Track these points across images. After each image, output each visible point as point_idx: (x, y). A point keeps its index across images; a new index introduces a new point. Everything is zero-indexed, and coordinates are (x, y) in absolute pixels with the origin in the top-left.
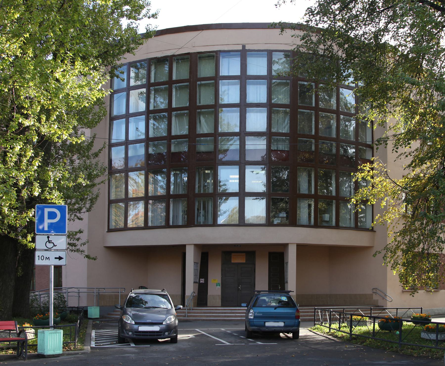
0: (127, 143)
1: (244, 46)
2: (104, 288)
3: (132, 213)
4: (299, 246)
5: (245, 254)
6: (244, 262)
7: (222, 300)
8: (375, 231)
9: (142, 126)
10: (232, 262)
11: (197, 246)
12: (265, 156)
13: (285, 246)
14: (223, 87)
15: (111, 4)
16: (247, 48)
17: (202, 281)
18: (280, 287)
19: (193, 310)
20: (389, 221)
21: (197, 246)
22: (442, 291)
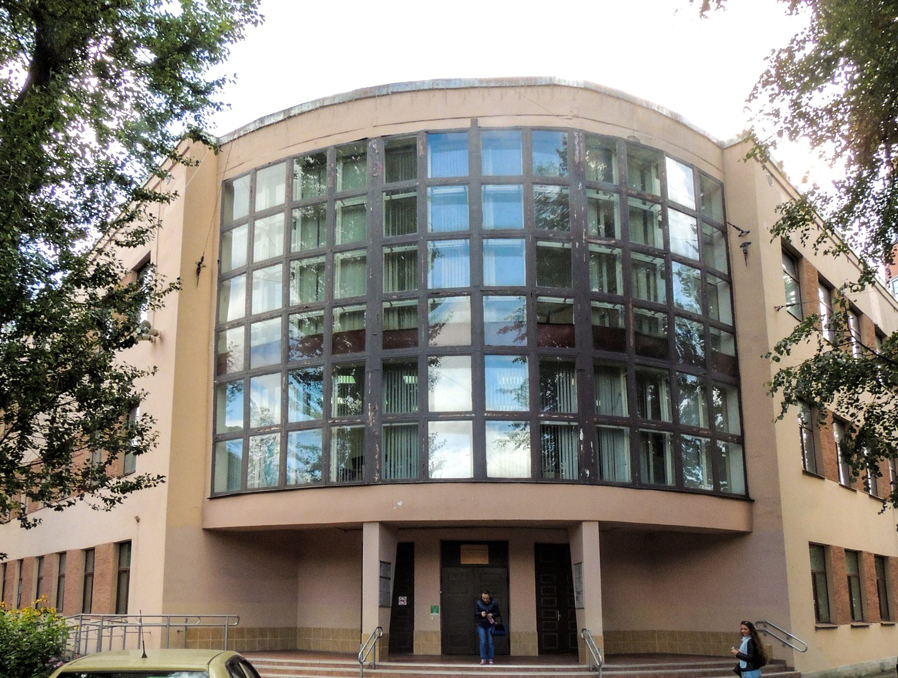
0: (248, 321)
2: (199, 617)
6: (487, 562)
7: (442, 641)
8: (753, 501)
10: (462, 563)
12: (178, 75)
16: (482, 123)
17: (403, 601)
18: (559, 616)
19: (375, 667)
20: (849, 107)
21: (388, 528)
22: (1, 79)
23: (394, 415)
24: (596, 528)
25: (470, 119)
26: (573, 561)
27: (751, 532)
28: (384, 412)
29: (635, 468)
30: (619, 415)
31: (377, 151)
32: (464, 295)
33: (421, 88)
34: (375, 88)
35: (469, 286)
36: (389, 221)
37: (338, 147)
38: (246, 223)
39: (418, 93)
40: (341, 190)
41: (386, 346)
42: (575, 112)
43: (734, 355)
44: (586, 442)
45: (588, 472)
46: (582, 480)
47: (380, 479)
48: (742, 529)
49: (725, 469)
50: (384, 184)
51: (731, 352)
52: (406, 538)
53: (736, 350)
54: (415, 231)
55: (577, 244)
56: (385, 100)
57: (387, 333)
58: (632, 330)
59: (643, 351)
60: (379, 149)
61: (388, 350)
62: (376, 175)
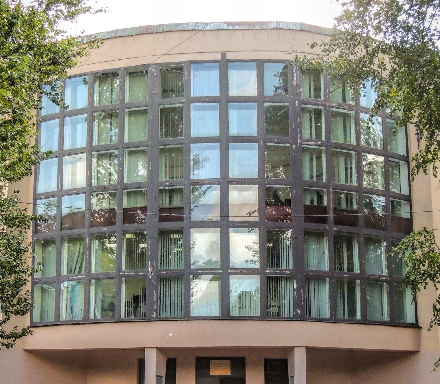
1: (224, 55)
3: (67, 170)
4: (310, 350)
5: (230, 361)
8: (421, 328)
9: (81, 166)
11: (160, 350)
13: (290, 350)
14: (195, 112)
15: (210, 224)
16: (229, 57)
23: (166, 270)
24: (304, 350)
25: (220, 53)
26: (289, 375)
27: (419, 351)
28: (159, 268)
29: (333, 308)
30: (323, 269)
31: (155, 74)
32: (215, 184)
33: (187, 29)
34: (154, 26)
35: (219, 177)
36: (162, 126)
37: (125, 68)
38: (58, 118)
39: (185, 32)
40: (128, 102)
41: (162, 219)
42: (294, 49)
43: (409, 217)
44: (298, 290)
45: (299, 312)
46: (296, 318)
47: (157, 317)
48: (412, 349)
49: (403, 303)
50: (158, 98)
51: (408, 216)
52: (171, 356)
53: (411, 214)
54: (181, 136)
55: (294, 146)
56: (161, 36)
57: (162, 210)
58: (331, 207)
59: (338, 221)
60: (157, 73)
61: (163, 223)
62: (155, 92)
